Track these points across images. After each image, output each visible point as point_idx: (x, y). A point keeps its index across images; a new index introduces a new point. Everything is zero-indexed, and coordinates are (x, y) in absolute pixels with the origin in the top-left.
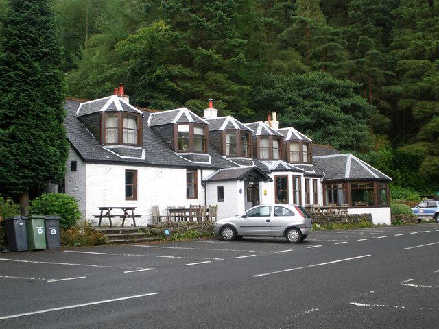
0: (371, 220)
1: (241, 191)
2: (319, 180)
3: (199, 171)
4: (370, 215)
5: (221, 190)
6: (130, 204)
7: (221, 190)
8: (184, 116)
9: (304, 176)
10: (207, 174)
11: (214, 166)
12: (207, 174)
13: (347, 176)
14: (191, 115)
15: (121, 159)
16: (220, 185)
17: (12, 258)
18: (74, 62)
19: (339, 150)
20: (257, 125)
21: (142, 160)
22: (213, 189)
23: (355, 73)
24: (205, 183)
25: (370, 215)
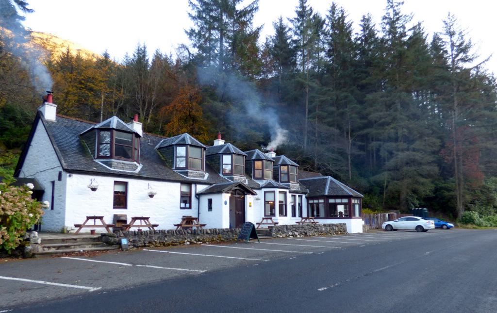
0: (345, 230)
1: (226, 203)
2: (304, 196)
3: (193, 186)
4: (345, 224)
5: (210, 201)
6: (120, 212)
7: (210, 201)
8: (283, 160)
9: (290, 192)
10: (201, 188)
11: (209, 182)
12: (201, 188)
13: (326, 194)
14: (233, 148)
15: (111, 171)
16: (210, 197)
17: (189, 272)
18: (96, 88)
19: (90, 120)
20: (280, 157)
21: (387, 213)
22: (204, 200)
23: (410, 147)
24: (198, 196)
25: (345, 224)
